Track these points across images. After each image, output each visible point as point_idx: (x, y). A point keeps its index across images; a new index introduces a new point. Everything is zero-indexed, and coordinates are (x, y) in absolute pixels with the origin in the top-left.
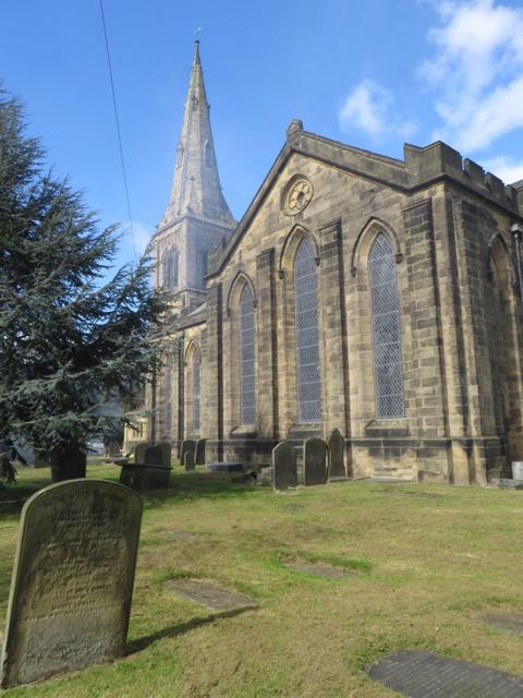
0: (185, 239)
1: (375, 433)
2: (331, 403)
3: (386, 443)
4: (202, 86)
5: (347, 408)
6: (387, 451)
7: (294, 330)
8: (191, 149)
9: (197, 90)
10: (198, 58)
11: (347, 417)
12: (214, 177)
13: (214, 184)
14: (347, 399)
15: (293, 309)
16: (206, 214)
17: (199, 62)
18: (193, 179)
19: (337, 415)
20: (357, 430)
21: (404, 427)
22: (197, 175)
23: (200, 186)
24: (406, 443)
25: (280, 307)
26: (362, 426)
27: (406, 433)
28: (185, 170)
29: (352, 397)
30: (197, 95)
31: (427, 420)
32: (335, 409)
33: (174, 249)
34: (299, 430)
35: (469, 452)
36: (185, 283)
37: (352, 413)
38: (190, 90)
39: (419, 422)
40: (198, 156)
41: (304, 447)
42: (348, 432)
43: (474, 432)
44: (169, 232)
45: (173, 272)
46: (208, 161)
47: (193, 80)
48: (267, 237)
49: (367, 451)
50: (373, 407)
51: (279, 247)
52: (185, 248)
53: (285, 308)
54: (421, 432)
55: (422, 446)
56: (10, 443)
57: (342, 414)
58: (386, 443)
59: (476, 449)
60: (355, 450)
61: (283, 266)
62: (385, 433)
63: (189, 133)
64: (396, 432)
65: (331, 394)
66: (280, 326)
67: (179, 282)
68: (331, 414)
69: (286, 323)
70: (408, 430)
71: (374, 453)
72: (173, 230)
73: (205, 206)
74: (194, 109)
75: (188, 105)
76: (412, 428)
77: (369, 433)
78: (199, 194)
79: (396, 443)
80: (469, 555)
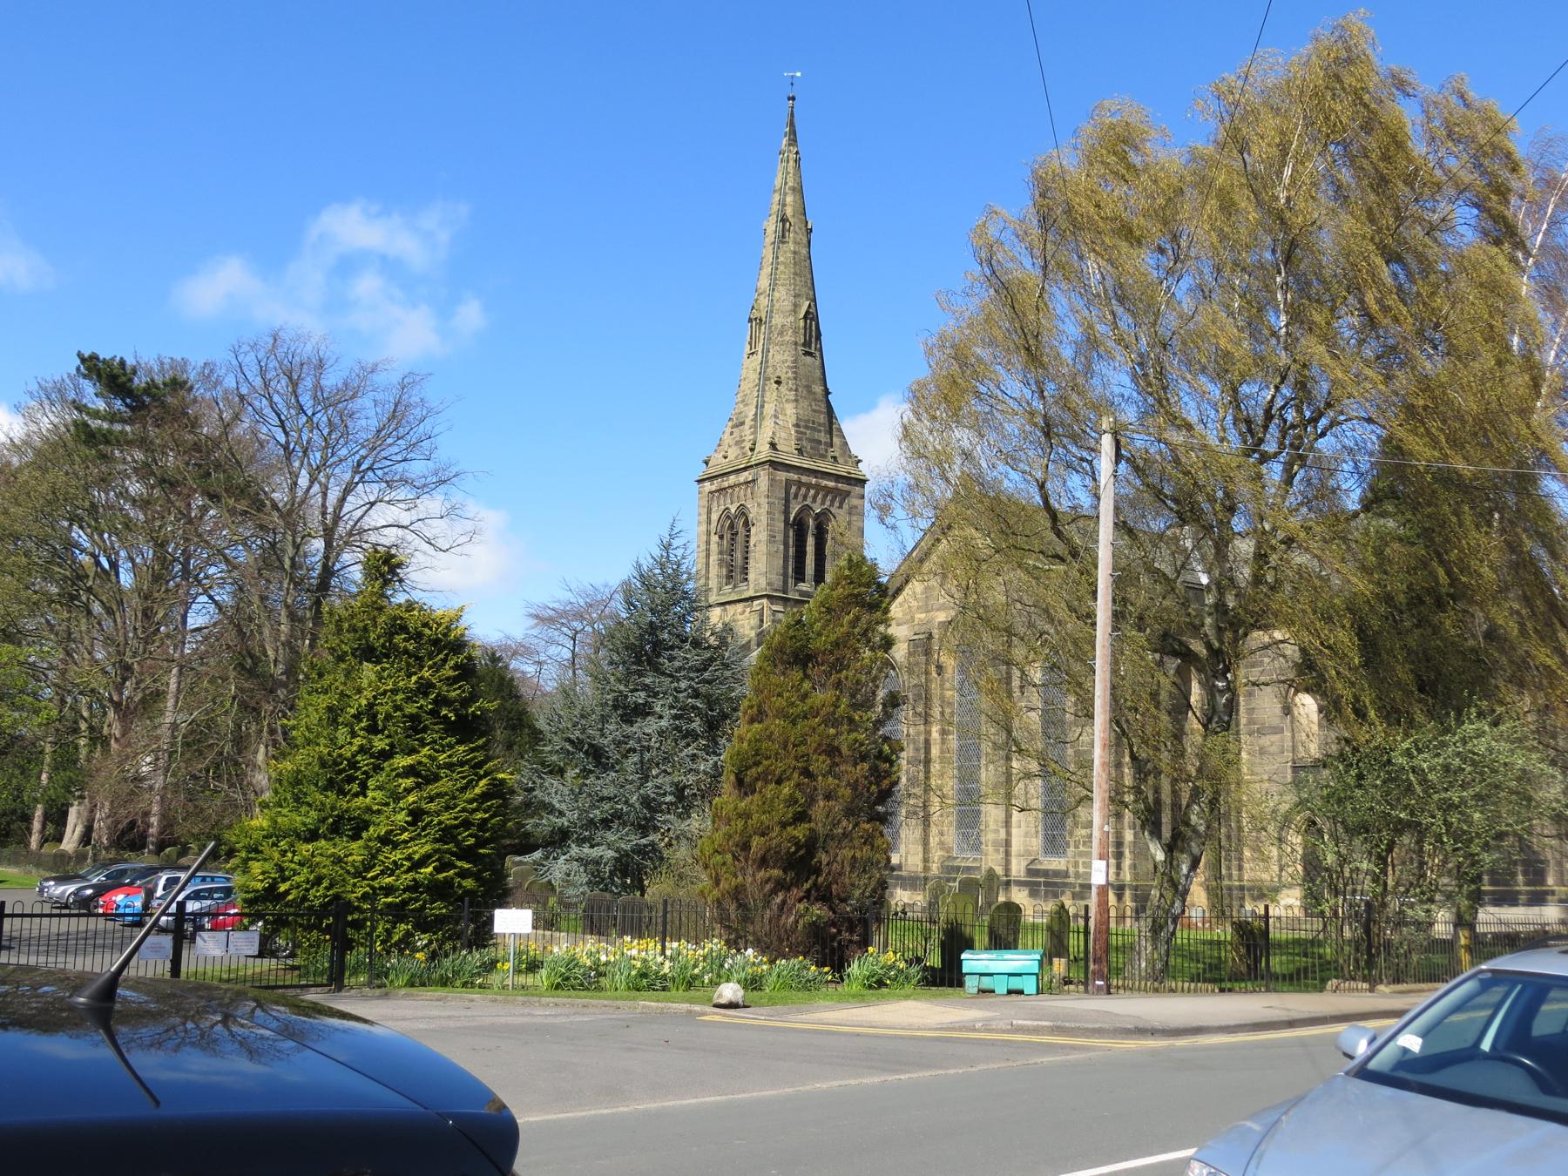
0: (764, 501)
1: (1035, 873)
2: (991, 836)
3: (1047, 884)
4: (799, 190)
5: (1008, 843)
6: (1046, 892)
7: (953, 741)
8: (778, 320)
9: (789, 199)
10: (793, 132)
11: (1008, 854)
12: (818, 373)
13: (818, 389)
14: (1009, 833)
15: (952, 714)
16: (800, 451)
17: (793, 141)
18: (778, 382)
19: (998, 851)
20: (1018, 868)
21: (1065, 868)
22: (785, 373)
23: (791, 395)
24: (1065, 885)
25: (936, 712)
26: (1024, 864)
27: (1066, 874)
28: (764, 363)
29: (1014, 831)
30: (789, 211)
31: (1084, 863)
32: (996, 844)
33: (743, 512)
34: (956, 863)
35: (1120, 897)
36: (763, 582)
37: (1014, 849)
38: (776, 197)
39: (1076, 865)
40: (789, 337)
41: (957, 884)
42: (1007, 870)
43: (1127, 876)
44: (732, 479)
45: (739, 555)
46: (807, 344)
47: (781, 176)
48: (923, 616)
49: (1027, 892)
50: (1037, 843)
51: (936, 633)
52: (764, 519)
53: (942, 713)
54: (1077, 875)
55: (1077, 889)
56: (1198, 962)
57: (1002, 849)
58: (1047, 884)
59: (1128, 894)
60: (1014, 889)
61: (942, 659)
62: (1046, 873)
63: (773, 287)
64: (1057, 873)
65: (992, 826)
66: (935, 735)
67: (751, 576)
68: (990, 848)
69: (944, 732)
70: (1067, 872)
71: (1034, 894)
72: (743, 477)
73: (800, 436)
74: (782, 238)
75: (771, 225)
76: (1071, 870)
77: (1030, 872)
78: (790, 410)
79: (1055, 884)
80: (199, 616)
